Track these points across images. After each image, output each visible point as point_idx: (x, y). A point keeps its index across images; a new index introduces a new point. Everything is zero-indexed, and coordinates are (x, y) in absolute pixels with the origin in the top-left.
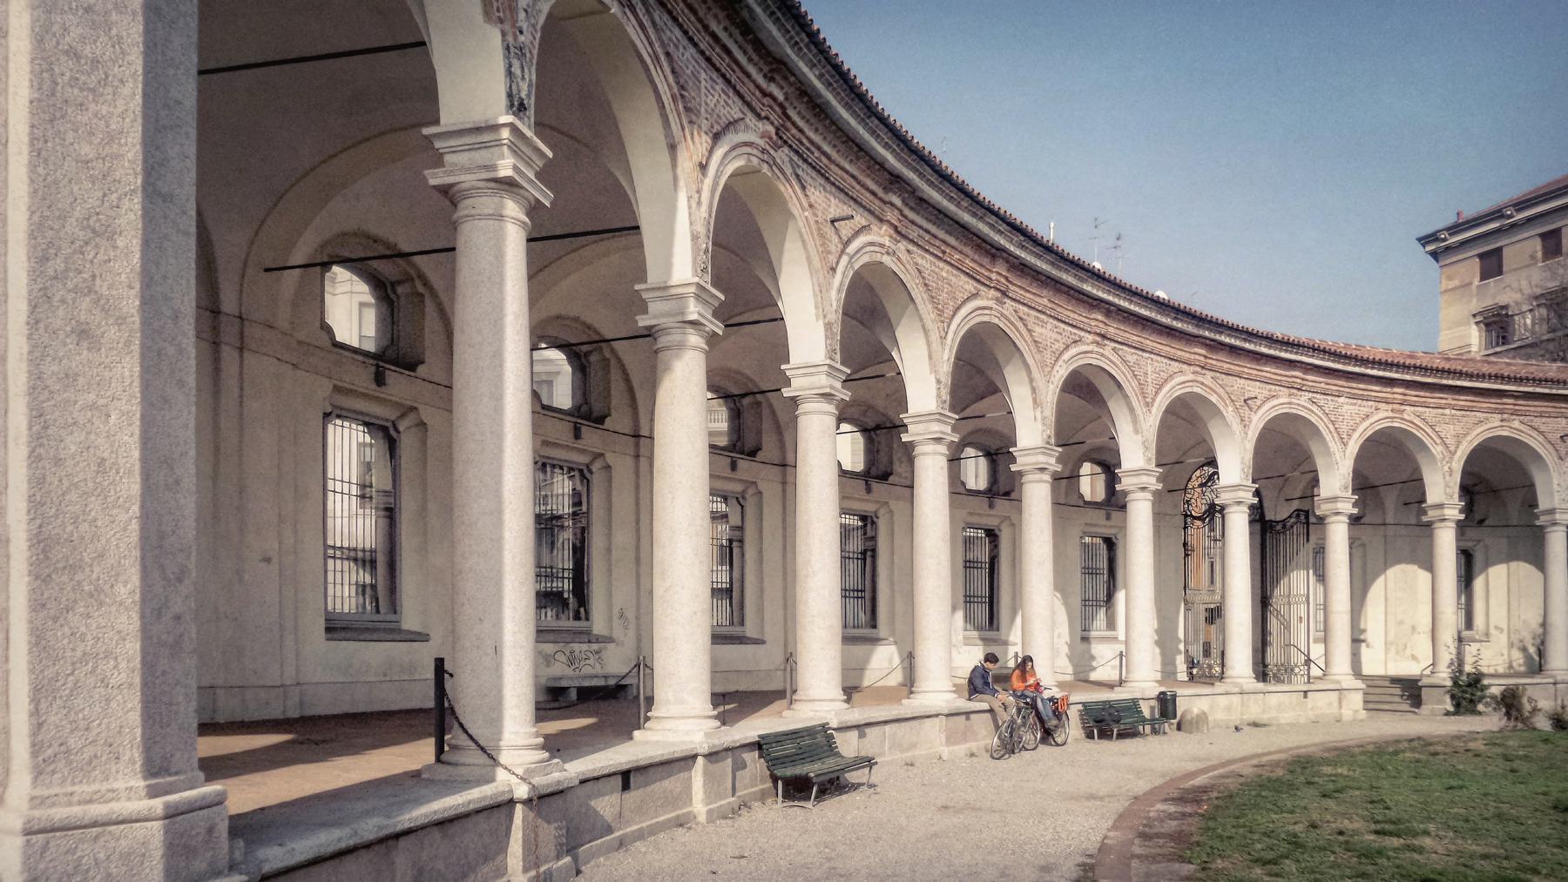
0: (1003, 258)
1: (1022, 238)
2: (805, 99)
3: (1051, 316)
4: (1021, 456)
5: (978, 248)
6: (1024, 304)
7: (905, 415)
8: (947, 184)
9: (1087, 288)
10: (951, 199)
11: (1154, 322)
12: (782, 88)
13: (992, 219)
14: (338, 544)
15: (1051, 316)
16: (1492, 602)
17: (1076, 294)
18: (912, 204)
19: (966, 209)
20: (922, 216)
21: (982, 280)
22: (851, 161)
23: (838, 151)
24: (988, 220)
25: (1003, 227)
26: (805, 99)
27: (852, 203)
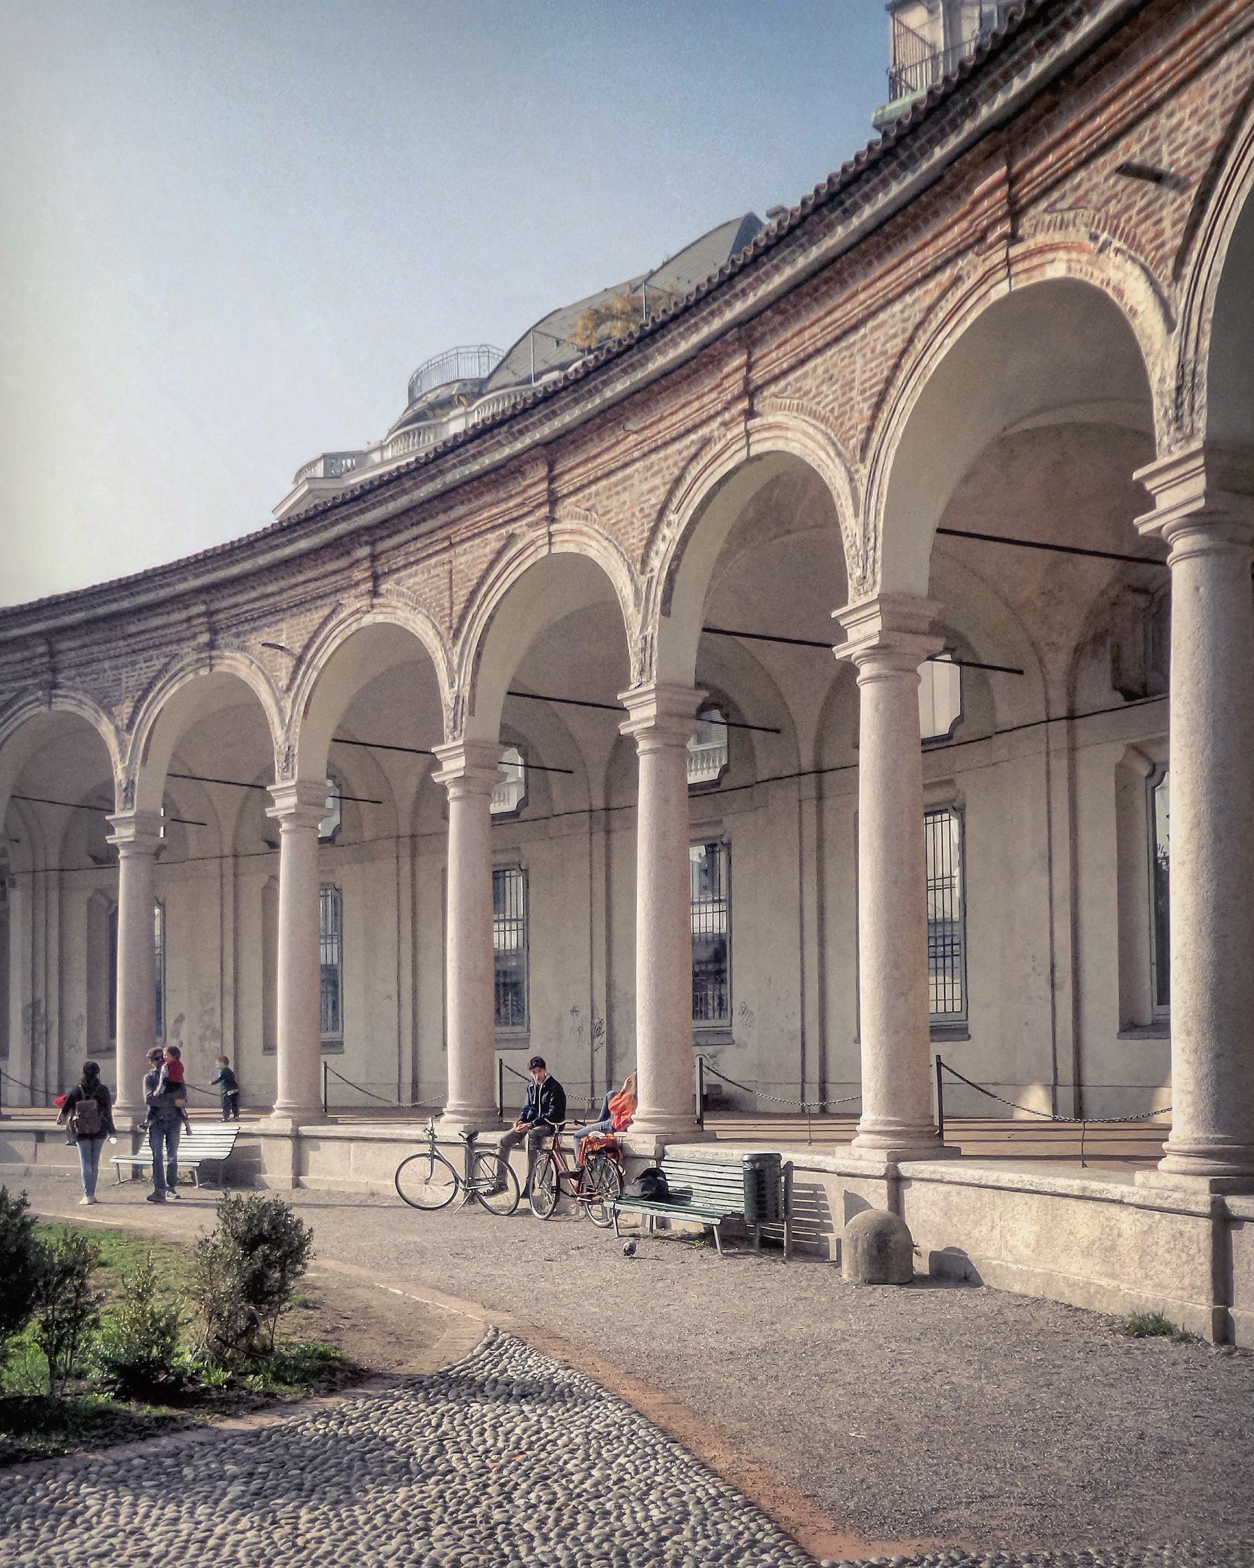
0: (527, 462)
1: (505, 428)
2: (1063, 83)
3: (645, 455)
4: (279, 797)
5: (495, 485)
6: (597, 480)
7: (626, 694)
8: (370, 496)
9: (659, 362)
10: (393, 498)
11: (828, 263)
12: (196, 604)
13: (451, 459)
14: (514, 917)
15: (645, 455)
16: (1085, 802)
17: (684, 371)
18: (385, 533)
19: (417, 486)
20: (407, 528)
21: (515, 514)
22: (300, 572)
23: (283, 578)
24: (448, 465)
25: (472, 449)
26: (1063, 83)
27: (319, 602)
